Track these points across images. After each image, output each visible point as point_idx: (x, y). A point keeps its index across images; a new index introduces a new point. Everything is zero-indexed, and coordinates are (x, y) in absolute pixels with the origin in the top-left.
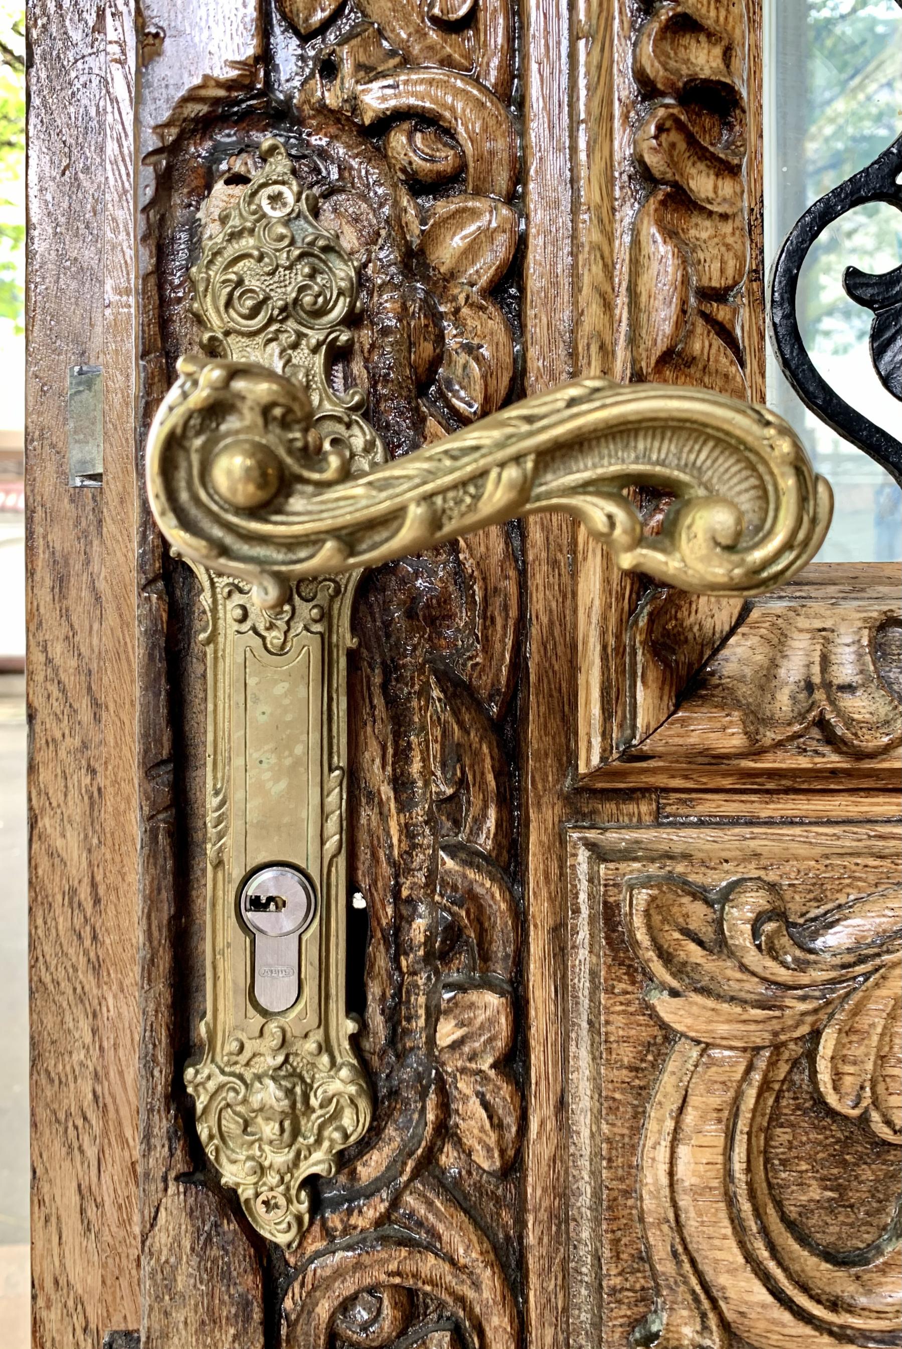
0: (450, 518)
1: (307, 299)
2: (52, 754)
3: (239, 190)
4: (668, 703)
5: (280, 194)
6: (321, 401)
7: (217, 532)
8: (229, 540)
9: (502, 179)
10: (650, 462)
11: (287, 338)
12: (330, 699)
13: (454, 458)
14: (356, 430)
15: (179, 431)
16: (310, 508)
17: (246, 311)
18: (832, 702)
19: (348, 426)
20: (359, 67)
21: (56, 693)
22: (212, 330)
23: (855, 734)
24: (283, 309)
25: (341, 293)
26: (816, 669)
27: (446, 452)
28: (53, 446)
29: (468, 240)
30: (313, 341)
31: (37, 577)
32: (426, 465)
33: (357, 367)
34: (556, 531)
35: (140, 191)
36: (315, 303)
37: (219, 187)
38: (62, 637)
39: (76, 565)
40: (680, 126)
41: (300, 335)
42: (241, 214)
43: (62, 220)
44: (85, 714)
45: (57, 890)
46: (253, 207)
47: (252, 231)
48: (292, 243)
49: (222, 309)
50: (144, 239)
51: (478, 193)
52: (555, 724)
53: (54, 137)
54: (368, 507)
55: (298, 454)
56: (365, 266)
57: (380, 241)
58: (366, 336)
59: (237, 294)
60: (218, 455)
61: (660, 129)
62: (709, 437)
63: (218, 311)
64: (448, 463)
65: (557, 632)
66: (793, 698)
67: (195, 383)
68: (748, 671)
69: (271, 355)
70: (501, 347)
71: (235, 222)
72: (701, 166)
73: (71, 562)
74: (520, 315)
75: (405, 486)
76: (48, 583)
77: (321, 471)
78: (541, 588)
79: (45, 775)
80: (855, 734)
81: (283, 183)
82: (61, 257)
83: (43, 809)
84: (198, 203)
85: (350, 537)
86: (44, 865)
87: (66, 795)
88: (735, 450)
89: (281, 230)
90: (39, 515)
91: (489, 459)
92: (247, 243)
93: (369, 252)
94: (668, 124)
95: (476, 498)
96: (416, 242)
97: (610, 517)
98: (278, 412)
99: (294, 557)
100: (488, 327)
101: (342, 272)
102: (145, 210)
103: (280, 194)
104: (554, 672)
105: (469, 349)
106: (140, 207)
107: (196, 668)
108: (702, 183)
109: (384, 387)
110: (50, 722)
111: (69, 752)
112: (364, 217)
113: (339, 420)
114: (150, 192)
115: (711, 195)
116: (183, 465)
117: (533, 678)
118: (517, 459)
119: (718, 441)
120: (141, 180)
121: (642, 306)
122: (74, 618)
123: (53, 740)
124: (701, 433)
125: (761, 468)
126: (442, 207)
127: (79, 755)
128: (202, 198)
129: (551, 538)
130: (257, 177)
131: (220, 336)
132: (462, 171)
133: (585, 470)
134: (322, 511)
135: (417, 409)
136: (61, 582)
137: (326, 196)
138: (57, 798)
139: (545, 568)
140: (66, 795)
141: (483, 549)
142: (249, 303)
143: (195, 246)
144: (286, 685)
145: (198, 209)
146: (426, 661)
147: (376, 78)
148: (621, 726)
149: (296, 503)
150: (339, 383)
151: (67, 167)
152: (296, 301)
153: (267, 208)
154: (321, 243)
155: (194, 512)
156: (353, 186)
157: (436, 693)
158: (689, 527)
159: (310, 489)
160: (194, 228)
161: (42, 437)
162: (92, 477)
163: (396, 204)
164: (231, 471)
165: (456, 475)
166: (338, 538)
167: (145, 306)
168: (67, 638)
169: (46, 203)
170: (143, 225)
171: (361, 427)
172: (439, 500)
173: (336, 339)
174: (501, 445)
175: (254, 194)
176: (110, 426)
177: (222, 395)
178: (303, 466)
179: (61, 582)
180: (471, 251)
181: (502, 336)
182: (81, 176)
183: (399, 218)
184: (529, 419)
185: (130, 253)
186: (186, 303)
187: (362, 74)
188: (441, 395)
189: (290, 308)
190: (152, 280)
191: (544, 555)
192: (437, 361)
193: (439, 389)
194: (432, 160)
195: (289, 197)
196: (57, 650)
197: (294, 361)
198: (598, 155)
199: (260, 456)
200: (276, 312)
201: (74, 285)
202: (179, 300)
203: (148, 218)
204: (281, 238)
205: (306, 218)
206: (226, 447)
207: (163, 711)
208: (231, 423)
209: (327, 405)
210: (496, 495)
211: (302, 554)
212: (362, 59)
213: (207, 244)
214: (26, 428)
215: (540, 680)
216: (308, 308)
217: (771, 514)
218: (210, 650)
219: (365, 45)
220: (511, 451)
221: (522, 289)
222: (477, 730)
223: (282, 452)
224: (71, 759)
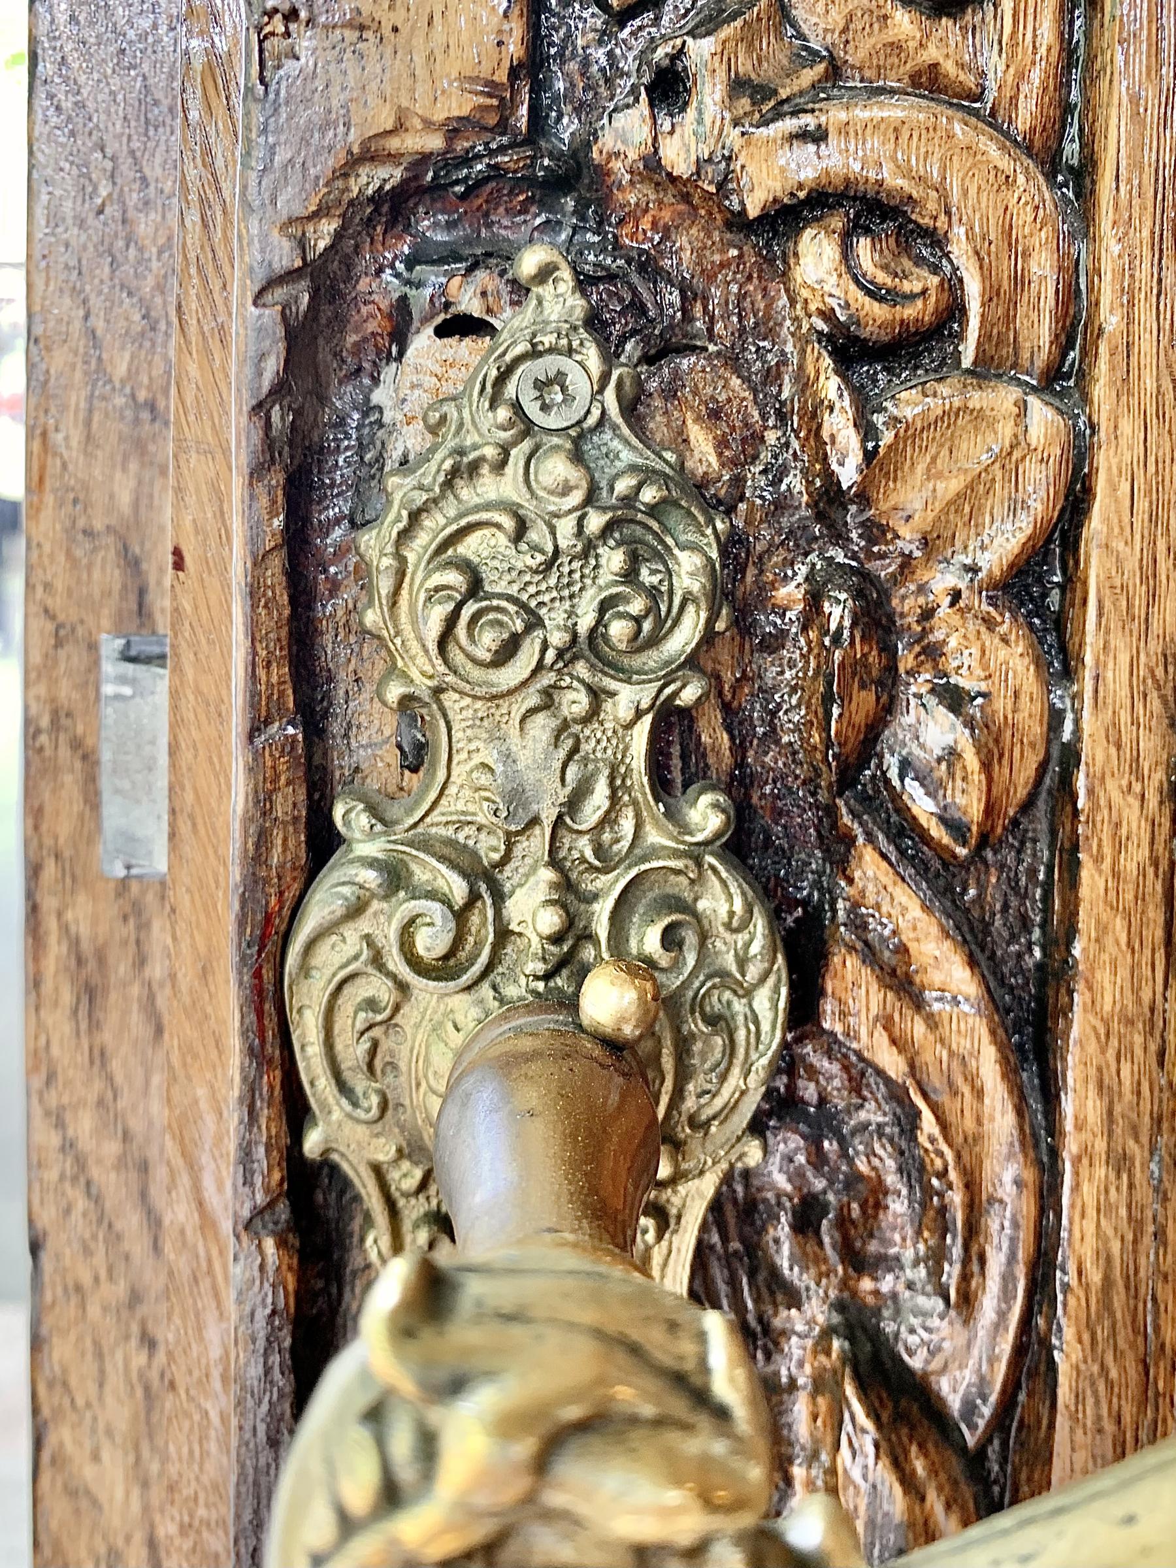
2: (72, 1310)
3: (465, 349)
5: (559, 379)
6: (638, 827)
9: (1038, 333)
17: (487, 657)
20: (738, 86)
21: (81, 1204)
28: (76, 744)
31: (48, 986)
34: (1128, 1096)
38: (92, 1098)
39: (121, 967)
41: (597, 695)
44: (137, 1245)
45: (83, 1554)
46: (503, 413)
48: (590, 499)
51: (986, 370)
70: (1024, 699)
73: (111, 960)
76: (67, 997)
78: (1091, 1212)
79: (60, 1351)
81: (570, 352)
83: (58, 1412)
86: (58, 1509)
87: (101, 1385)
90: (50, 870)
100: (993, 659)
103: (559, 379)
111: (105, 1309)
122: (115, 1065)
123: (78, 1288)
126: (909, 403)
127: (125, 1314)
129: (1118, 1109)
132: (951, 318)
136: (91, 995)
138: (85, 1390)
139: (1101, 1172)
140: (101, 1385)
141: (969, 1124)
145: (376, 381)
147: (778, 115)
156: (711, 337)
168: (101, 1103)
175: (504, 376)
179: (91, 995)
180: (968, 503)
187: (745, 103)
191: (1100, 1145)
195: (580, 385)
196: (84, 1125)
197: (586, 747)
205: (615, 428)
212: (744, 65)
214: (26, 708)
215: (1078, 1397)
219: (749, 37)
222: (940, 1489)
224: (110, 1321)
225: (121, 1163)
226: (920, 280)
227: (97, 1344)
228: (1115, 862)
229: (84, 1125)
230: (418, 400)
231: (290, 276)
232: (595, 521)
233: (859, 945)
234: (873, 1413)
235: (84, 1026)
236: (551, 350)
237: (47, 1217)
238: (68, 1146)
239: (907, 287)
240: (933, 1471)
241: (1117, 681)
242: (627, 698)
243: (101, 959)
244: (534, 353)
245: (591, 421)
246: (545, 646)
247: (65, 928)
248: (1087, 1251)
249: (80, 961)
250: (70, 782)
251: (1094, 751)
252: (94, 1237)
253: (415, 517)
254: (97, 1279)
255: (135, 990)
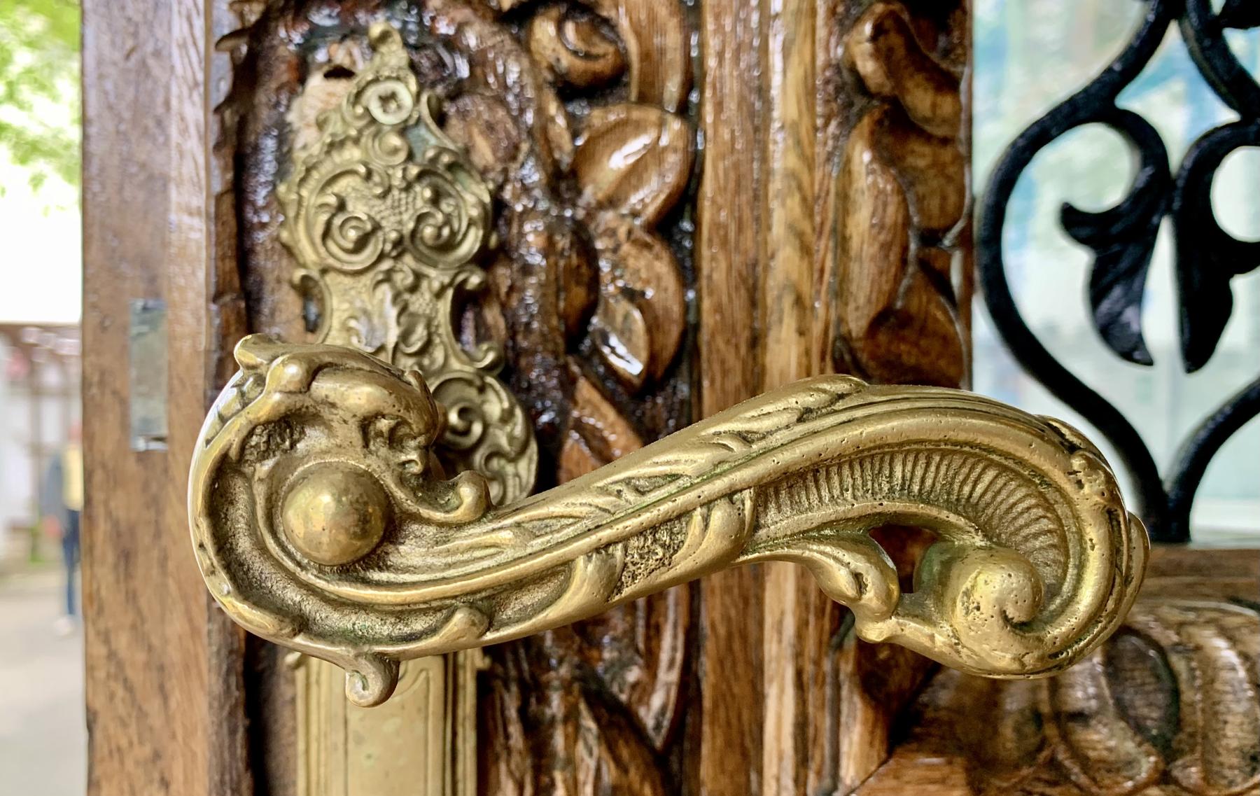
0: (634, 577)
1: (428, 232)
2: (116, 764)
3: (342, 88)
4: (878, 751)
6: (446, 358)
7: (292, 595)
8: (311, 606)
9: (672, 88)
10: (910, 497)
11: (404, 279)
12: (454, 734)
13: (640, 492)
14: (491, 395)
15: (233, 453)
16: (430, 560)
17: (350, 246)
18: (1065, 737)
19: (482, 389)
21: (120, 692)
22: (304, 266)
23: (1094, 780)
24: (398, 243)
25: (471, 223)
26: (1044, 695)
27: (628, 482)
28: (115, 393)
29: (632, 159)
30: (436, 285)
32: (602, 501)
33: (492, 315)
35: (212, 85)
36: (439, 235)
37: (316, 81)
39: (145, 538)
40: (901, 28)
41: (418, 276)
42: (343, 120)
43: (127, 115)
46: (360, 110)
47: (356, 141)
48: (410, 157)
49: (318, 240)
50: (218, 147)
52: (732, 761)
53: (116, 12)
54: (516, 560)
55: (414, 482)
56: (501, 188)
57: (521, 157)
58: (504, 275)
59: (338, 221)
60: (292, 488)
61: (878, 32)
62: (991, 464)
63: (313, 243)
64: (630, 496)
65: (737, 646)
66: (1018, 730)
67: (260, 381)
68: (967, 700)
69: (382, 301)
71: (335, 127)
72: (919, 78)
74: (694, 253)
75: (570, 531)
76: (110, 558)
77: (446, 508)
80: (1094, 780)
81: (398, 79)
82: (126, 160)
84: (290, 100)
85: (487, 604)
88: (1028, 482)
89: (395, 141)
90: (99, 476)
91: (691, 496)
92: (352, 154)
93: (505, 171)
94: (888, 24)
95: (672, 548)
96: (566, 160)
97: (857, 576)
98: (384, 425)
99: (407, 630)
100: (653, 271)
101: (472, 197)
102: (218, 110)
104: (733, 696)
105: (632, 295)
106: (213, 105)
107: (283, 691)
108: (921, 99)
109: (525, 338)
110: (113, 728)
111: (137, 763)
112: (499, 127)
113: (469, 383)
114: (225, 87)
115: (928, 114)
116: (242, 498)
117: (707, 703)
118: (730, 495)
119: (1004, 469)
120: (214, 70)
121: (853, 253)
122: (143, 602)
123: (119, 749)
124: (980, 459)
125: (1061, 510)
126: (598, 117)
128: (293, 94)
130: (364, 70)
131: (315, 274)
133: (823, 506)
134: (449, 566)
135: (565, 368)
137: (453, 97)
142: (353, 234)
143: (284, 158)
144: (398, 721)
145: (288, 107)
146: (574, 679)
148: (819, 773)
149: (410, 550)
150: (469, 335)
151: (133, 50)
152: (414, 233)
153: (377, 111)
154: (446, 159)
155: (258, 566)
157: (589, 723)
158: (967, 594)
159: (431, 531)
160: (284, 134)
161: (102, 383)
162: (160, 439)
163: (540, 111)
164: (315, 513)
165: (646, 517)
166: (471, 605)
167: (218, 235)
168: (134, 627)
169: (106, 93)
170: (215, 128)
171: (497, 393)
172: (618, 551)
173: (465, 281)
174: (709, 476)
175: (359, 95)
176: (176, 382)
177: (299, 401)
178: (420, 501)
180: (634, 174)
181: (670, 280)
182: (151, 62)
183: (545, 130)
184: (745, 438)
185: (201, 160)
186: (272, 230)
188: (596, 350)
189: (407, 242)
190: (228, 201)
192: (590, 308)
193: (593, 343)
194: (588, 56)
196: (122, 642)
197: (412, 308)
198: (795, 59)
199: (355, 492)
200: (388, 247)
201: (141, 196)
202: (263, 226)
203: (222, 122)
204: (395, 151)
205: (427, 126)
206: (304, 477)
207: (241, 752)
208: (313, 440)
209: (455, 364)
210: (703, 542)
211: (419, 625)
213: (300, 155)
214: (84, 372)
215: (715, 706)
216: (430, 242)
217: (1071, 571)
218: (300, 674)
220: (720, 485)
221: (696, 222)
222: (638, 768)
223: (390, 482)
225: (147, 665)
226: (602, 48)
227: (132, 787)
228: (723, 384)
229: (122, 642)
230: (312, 115)
231: (234, 34)
232: (414, 171)
233: (676, 749)
234: (597, 719)
235: (122, 577)
236: (388, 78)
237: (99, 703)
238: (112, 655)
239: (595, 51)
240: (633, 757)
241: (719, 276)
242: (437, 277)
243: (132, 530)
244: (376, 80)
245: (412, 122)
246: (385, 241)
247: (109, 514)
248: (717, 615)
249: (119, 535)
250: (112, 418)
251: (709, 319)
252: (129, 715)
253: (308, 170)
254: (131, 744)
255: (155, 553)
